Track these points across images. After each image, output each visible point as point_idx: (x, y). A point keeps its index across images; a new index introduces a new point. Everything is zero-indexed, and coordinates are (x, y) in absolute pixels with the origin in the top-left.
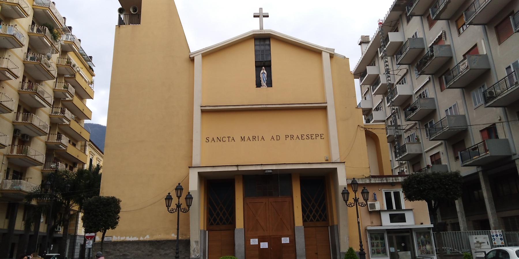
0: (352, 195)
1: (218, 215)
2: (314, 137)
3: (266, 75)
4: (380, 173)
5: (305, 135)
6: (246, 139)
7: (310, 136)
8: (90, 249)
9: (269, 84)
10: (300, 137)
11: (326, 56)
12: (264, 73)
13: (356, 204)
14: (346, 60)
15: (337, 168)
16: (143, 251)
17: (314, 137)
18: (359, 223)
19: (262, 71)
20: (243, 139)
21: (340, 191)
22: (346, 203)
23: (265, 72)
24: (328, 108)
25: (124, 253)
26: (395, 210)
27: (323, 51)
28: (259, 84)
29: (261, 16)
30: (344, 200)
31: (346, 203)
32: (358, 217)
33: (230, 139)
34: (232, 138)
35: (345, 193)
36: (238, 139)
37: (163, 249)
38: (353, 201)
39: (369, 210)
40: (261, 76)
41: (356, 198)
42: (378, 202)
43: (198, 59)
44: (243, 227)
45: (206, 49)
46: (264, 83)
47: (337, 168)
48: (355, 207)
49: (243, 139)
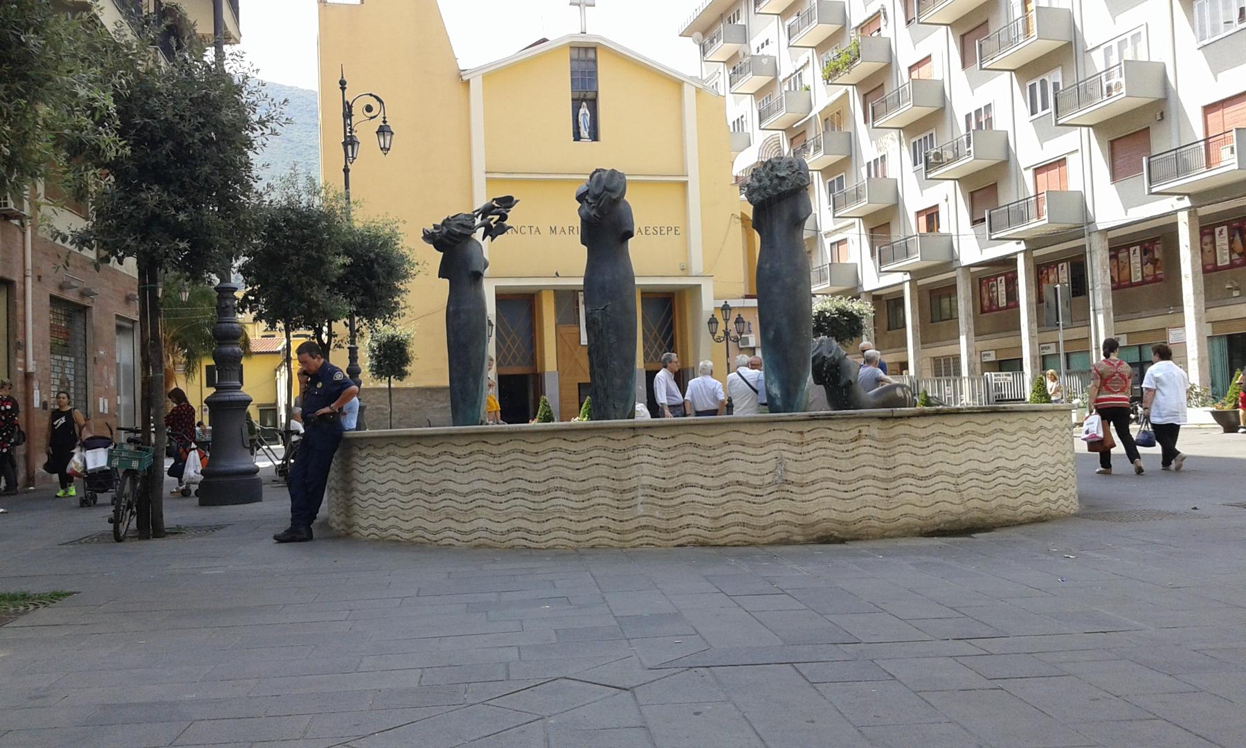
0: (721, 326)
1: (509, 349)
2: (665, 231)
3: (588, 118)
4: (1114, 455)
5: (652, 228)
6: (558, 230)
7: (658, 230)
8: (118, 394)
9: (594, 136)
10: (643, 231)
11: (689, 92)
12: (585, 114)
13: (727, 339)
14: (697, 77)
15: (700, 285)
16: (407, 404)
17: (665, 231)
18: (728, 364)
19: (581, 110)
20: (553, 230)
21: (705, 318)
22: (713, 336)
23: (588, 112)
24: (689, 184)
25: (378, 406)
26: (547, 287)
27: (685, 84)
28: (577, 137)
29: (582, 6)
30: (711, 333)
31: (713, 336)
32: (728, 356)
33: (533, 230)
34: (535, 227)
35: (713, 321)
36: (545, 230)
37: (437, 400)
38: (722, 334)
39: (740, 346)
40: (581, 119)
41: (727, 329)
42: (753, 335)
43: (476, 86)
44: (556, 369)
45: (491, 65)
46: (584, 133)
47: (700, 285)
48: (725, 342)
49: (553, 230)
